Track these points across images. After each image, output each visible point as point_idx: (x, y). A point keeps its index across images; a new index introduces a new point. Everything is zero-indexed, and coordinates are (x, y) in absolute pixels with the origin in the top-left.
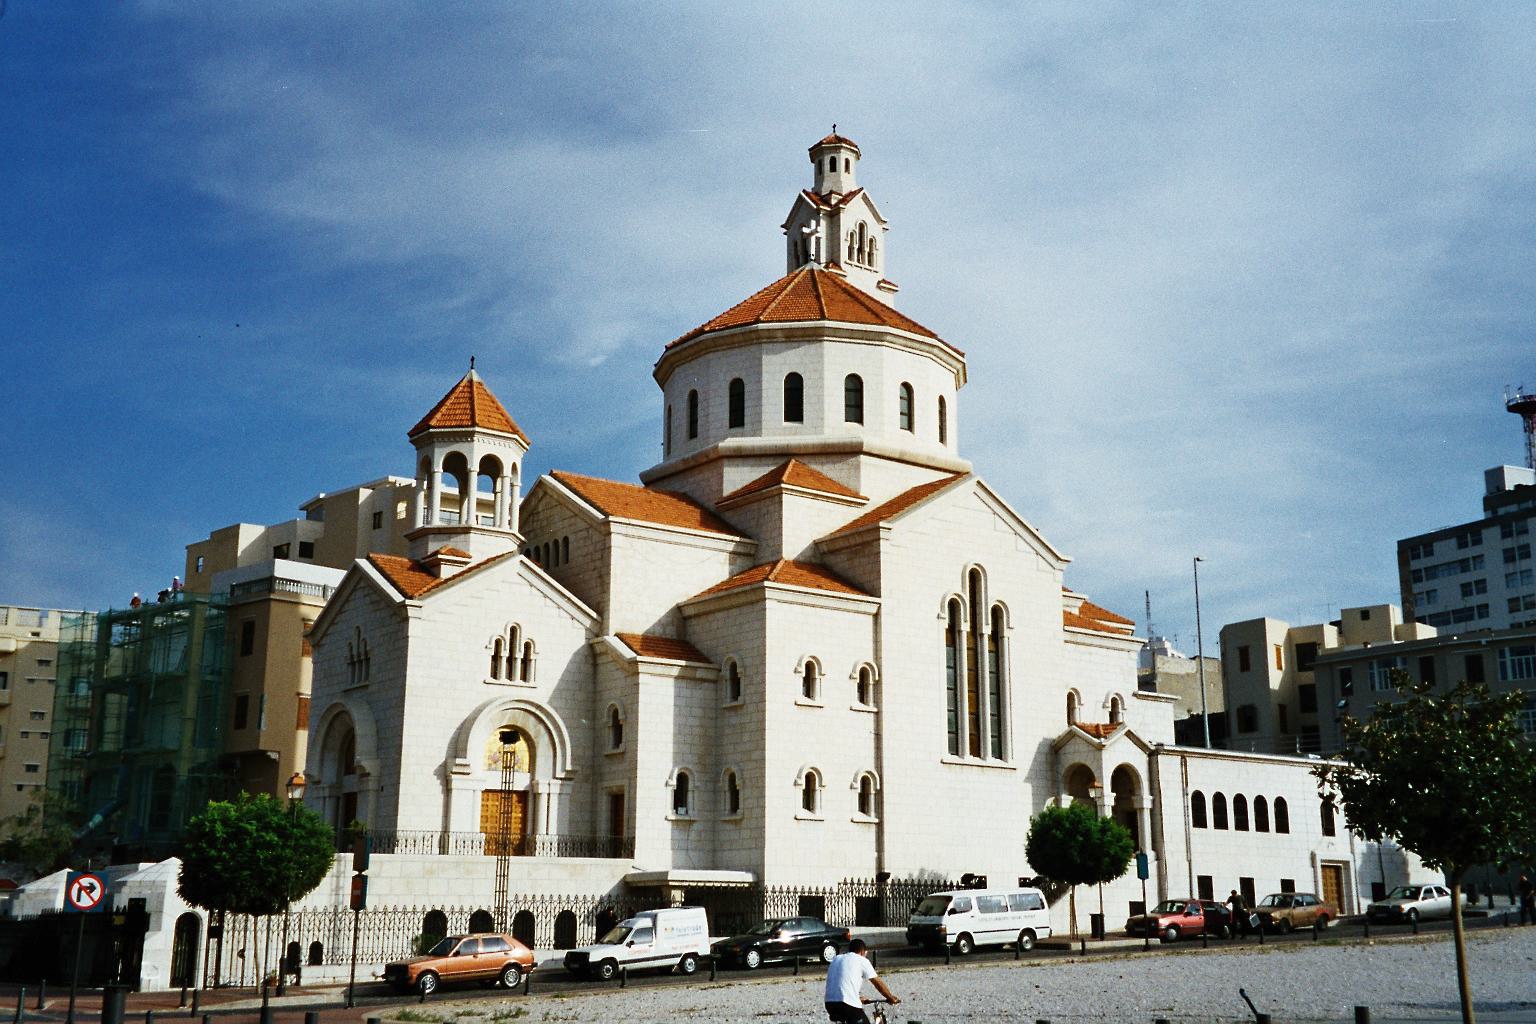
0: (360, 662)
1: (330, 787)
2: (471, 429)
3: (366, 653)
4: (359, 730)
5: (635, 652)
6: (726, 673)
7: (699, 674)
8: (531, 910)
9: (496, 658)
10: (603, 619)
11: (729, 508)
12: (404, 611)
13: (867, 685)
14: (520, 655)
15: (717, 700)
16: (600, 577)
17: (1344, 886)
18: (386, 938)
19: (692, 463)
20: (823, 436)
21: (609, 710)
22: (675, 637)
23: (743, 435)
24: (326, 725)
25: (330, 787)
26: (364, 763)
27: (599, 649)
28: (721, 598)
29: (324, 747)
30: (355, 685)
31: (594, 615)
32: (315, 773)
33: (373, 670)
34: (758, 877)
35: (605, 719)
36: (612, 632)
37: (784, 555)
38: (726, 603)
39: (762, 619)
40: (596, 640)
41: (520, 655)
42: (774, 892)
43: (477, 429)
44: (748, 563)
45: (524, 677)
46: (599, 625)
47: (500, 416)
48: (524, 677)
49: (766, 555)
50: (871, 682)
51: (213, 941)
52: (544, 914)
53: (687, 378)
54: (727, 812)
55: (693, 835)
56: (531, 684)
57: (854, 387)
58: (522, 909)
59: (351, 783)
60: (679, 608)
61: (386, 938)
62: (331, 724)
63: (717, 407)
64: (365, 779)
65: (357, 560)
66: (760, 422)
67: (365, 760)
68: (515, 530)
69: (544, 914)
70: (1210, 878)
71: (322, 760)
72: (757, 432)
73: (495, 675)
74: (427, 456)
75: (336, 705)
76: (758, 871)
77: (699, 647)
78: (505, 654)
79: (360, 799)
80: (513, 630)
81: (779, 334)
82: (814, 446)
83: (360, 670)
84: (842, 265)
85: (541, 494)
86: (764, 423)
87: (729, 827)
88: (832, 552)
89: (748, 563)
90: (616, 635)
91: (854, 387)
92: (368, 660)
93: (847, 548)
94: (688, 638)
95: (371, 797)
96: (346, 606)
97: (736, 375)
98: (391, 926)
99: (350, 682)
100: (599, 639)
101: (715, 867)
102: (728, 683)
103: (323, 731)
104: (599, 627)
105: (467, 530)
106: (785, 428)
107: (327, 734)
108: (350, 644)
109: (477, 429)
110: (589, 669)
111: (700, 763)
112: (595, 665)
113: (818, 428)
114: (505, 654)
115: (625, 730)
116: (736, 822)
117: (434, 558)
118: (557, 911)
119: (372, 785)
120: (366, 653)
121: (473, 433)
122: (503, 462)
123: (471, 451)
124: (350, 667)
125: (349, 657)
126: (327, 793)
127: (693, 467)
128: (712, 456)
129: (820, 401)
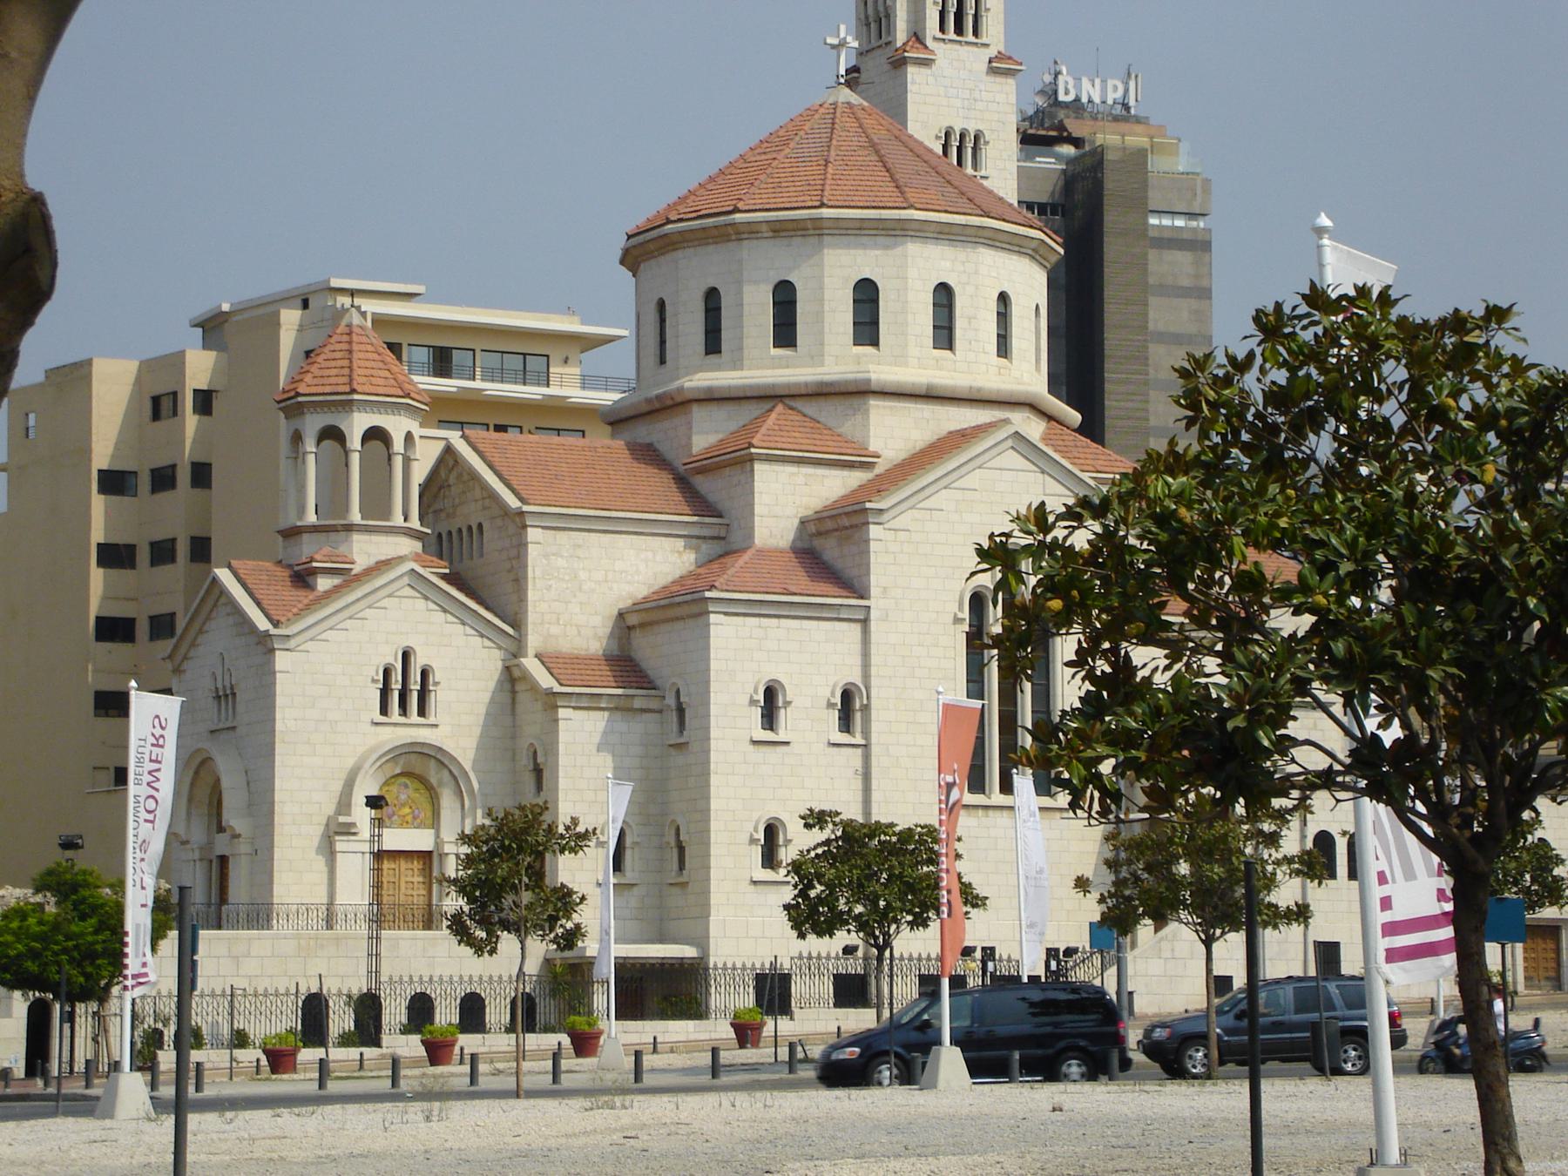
0: (226, 696)
1: (201, 848)
2: (350, 397)
3: (232, 688)
4: (225, 783)
5: (557, 680)
6: (671, 701)
7: (638, 703)
8: (428, 992)
9: (385, 692)
10: (520, 636)
11: (702, 471)
12: (269, 642)
13: (849, 707)
14: (415, 686)
15: (662, 734)
16: (517, 580)
17: (1564, 951)
18: (278, 1022)
19: (657, 405)
20: (820, 370)
21: (528, 750)
22: (616, 653)
23: (719, 368)
24: (191, 773)
25: (201, 848)
26: (233, 823)
27: (516, 673)
28: (663, 607)
29: (190, 800)
30: (221, 726)
31: (510, 630)
32: (181, 830)
33: (240, 708)
34: (703, 948)
35: (525, 761)
36: (531, 652)
37: (756, 541)
38: (671, 613)
39: (706, 637)
40: (515, 661)
41: (415, 686)
42: (716, 968)
43: (356, 397)
44: (717, 548)
45: (422, 712)
46: (517, 642)
47: (387, 374)
48: (422, 712)
49: (736, 538)
50: (857, 706)
51: (67, 1026)
52: (394, 997)
53: (656, 269)
54: (673, 873)
55: (633, 902)
56: (432, 720)
57: (866, 295)
58: (468, 991)
59: (221, 845)
60: (621, 615)
61: (278, 1022)
62: (197, 773)
63: (688, 326)
64: (236, 840)
65: (216, 570)
66: (741, 349)
67: (234, 818)
68: (415, 523)
69: (394, 997)
70: (1336, 945)
71: (189, 814)
72: (737, 364)
73: (384, 710)
74: (297, 430)
75: (198, 750)
76: (702, 942)
77: (644, 665)
78: (396, 685)
79: (231, 860)
80: (406, 656)
81: (764, 228)
82: (806, 384)
83: (227, 710)
84: (929, 42)
85: (451, 463)
86: (746, 352)
87: (675, 890)
88: (819, 534)
89: (717, 548)
90: (536, 656)
91: (866, 295)
92: (234, 694)
93: (836, 530)
94: (632, 654)
95: (244, 861)
96: (208, 624)
97: (712, 283)
98: (199, 1010)
99: (216, 721)
100: (515, 661)
101: (662, 939)
102: (674, 713)
103: (188, 780)
104: (516, 648)
105: (350, 528)
106: (773, 358)
107: (192, 785)
108: (214, 673)
109: (356, 397)
110: (506, 697)
111: (640, 814)
112: (514, 692)
113: (817, 357)
114: (396, 685)
115: (546, 774)
116: (684, 885)
117: (309, 565)
118: (408, 992)
119: (243, 847)
120: (232, 688)
121: (352, 401)
122: (392, 434)
123: (351, 426)
124: (216, 702)
125: (213, 688)
126: (197, 855)
127: (657, 411)
128: (679, 399)
129: (819, 316)
